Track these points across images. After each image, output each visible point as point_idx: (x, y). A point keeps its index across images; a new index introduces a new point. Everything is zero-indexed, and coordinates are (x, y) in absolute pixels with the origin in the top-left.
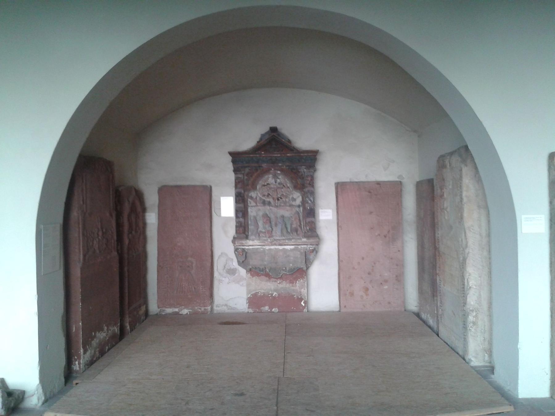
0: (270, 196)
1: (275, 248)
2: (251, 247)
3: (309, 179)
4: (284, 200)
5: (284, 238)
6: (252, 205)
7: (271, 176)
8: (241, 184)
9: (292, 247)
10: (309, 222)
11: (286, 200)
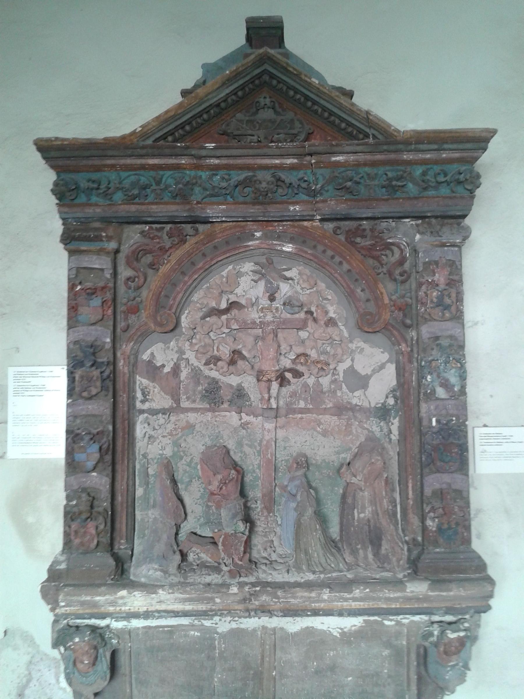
0: (240, 363)
1: (264, 628)
2: (137, 623)
3: (440, 278)
4: (311, 381)
6: (155, 405)
7: (248, 267)
8: (96, 302)
9: (357, 622)
10: (440, 494)
11: (318, 384)
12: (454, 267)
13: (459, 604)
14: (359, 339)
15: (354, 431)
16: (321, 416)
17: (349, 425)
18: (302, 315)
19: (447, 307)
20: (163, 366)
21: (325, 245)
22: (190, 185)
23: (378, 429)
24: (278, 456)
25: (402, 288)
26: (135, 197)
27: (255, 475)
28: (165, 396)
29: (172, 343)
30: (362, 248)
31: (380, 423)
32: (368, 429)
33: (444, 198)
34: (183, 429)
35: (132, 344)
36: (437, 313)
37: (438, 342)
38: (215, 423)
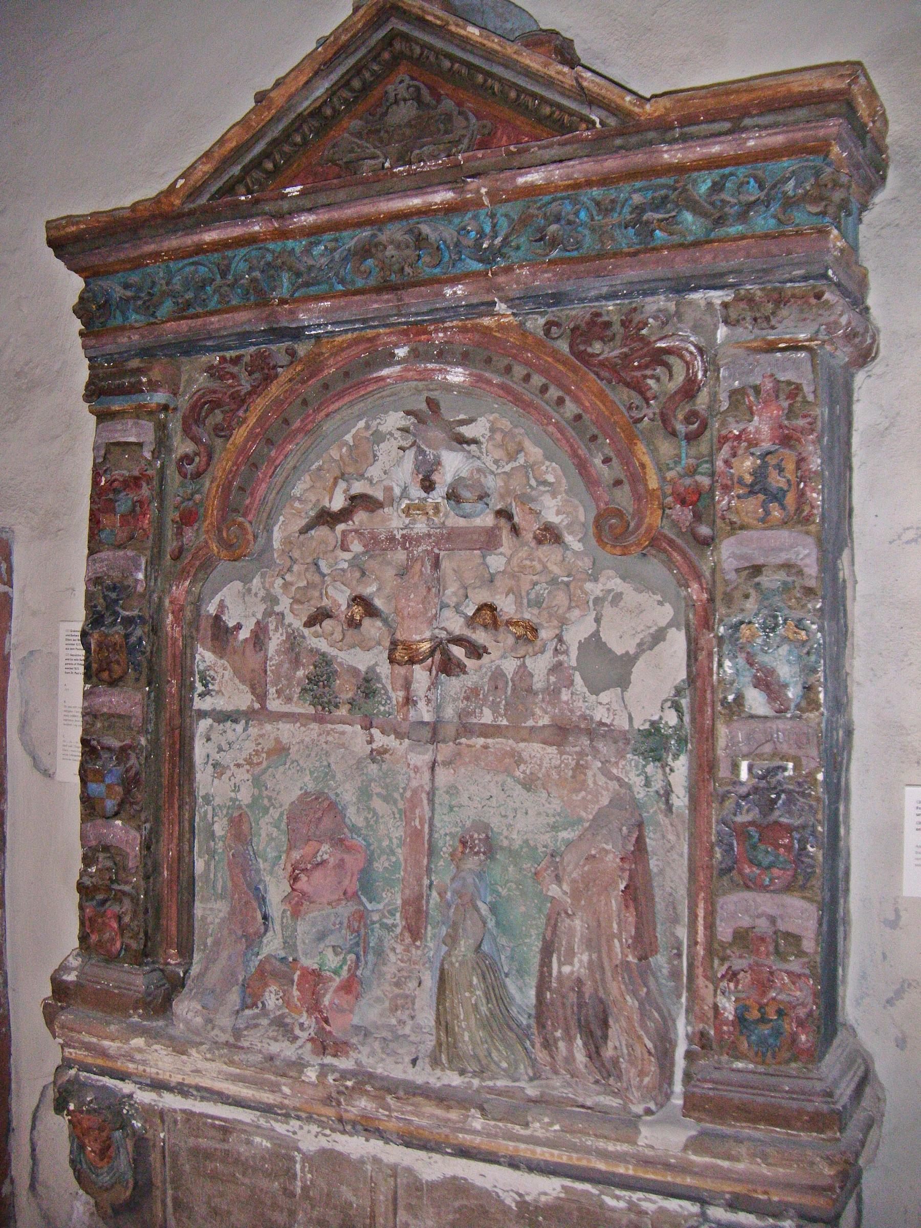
1: (376, 1160)
4: (510, 666)
5: (454, 1080)
11: (523, 673)
12: (799, 399)
13: (765, 1193)
14: (611, 573)
15: (590, 782)
16: (522, 745)
17: (580, 768)
18: (487, 520)
19: (777, 497)
20: (239, 627)
21: (527, 363)
22: (272, 269)
23: (640, 781)
24: (437, 823)
25: (693, 452)
26: (188, 304)
27: (394, 859)
28: (242, 687)
29: (255, 581)
30: (602, 364)
31: (644, 766)
32: (618, 779)
33: (766, 236)
34: (269, 753)
35: (187, 583)
36: (752, 506)
37: (757, 580)
38: (324, 746)
